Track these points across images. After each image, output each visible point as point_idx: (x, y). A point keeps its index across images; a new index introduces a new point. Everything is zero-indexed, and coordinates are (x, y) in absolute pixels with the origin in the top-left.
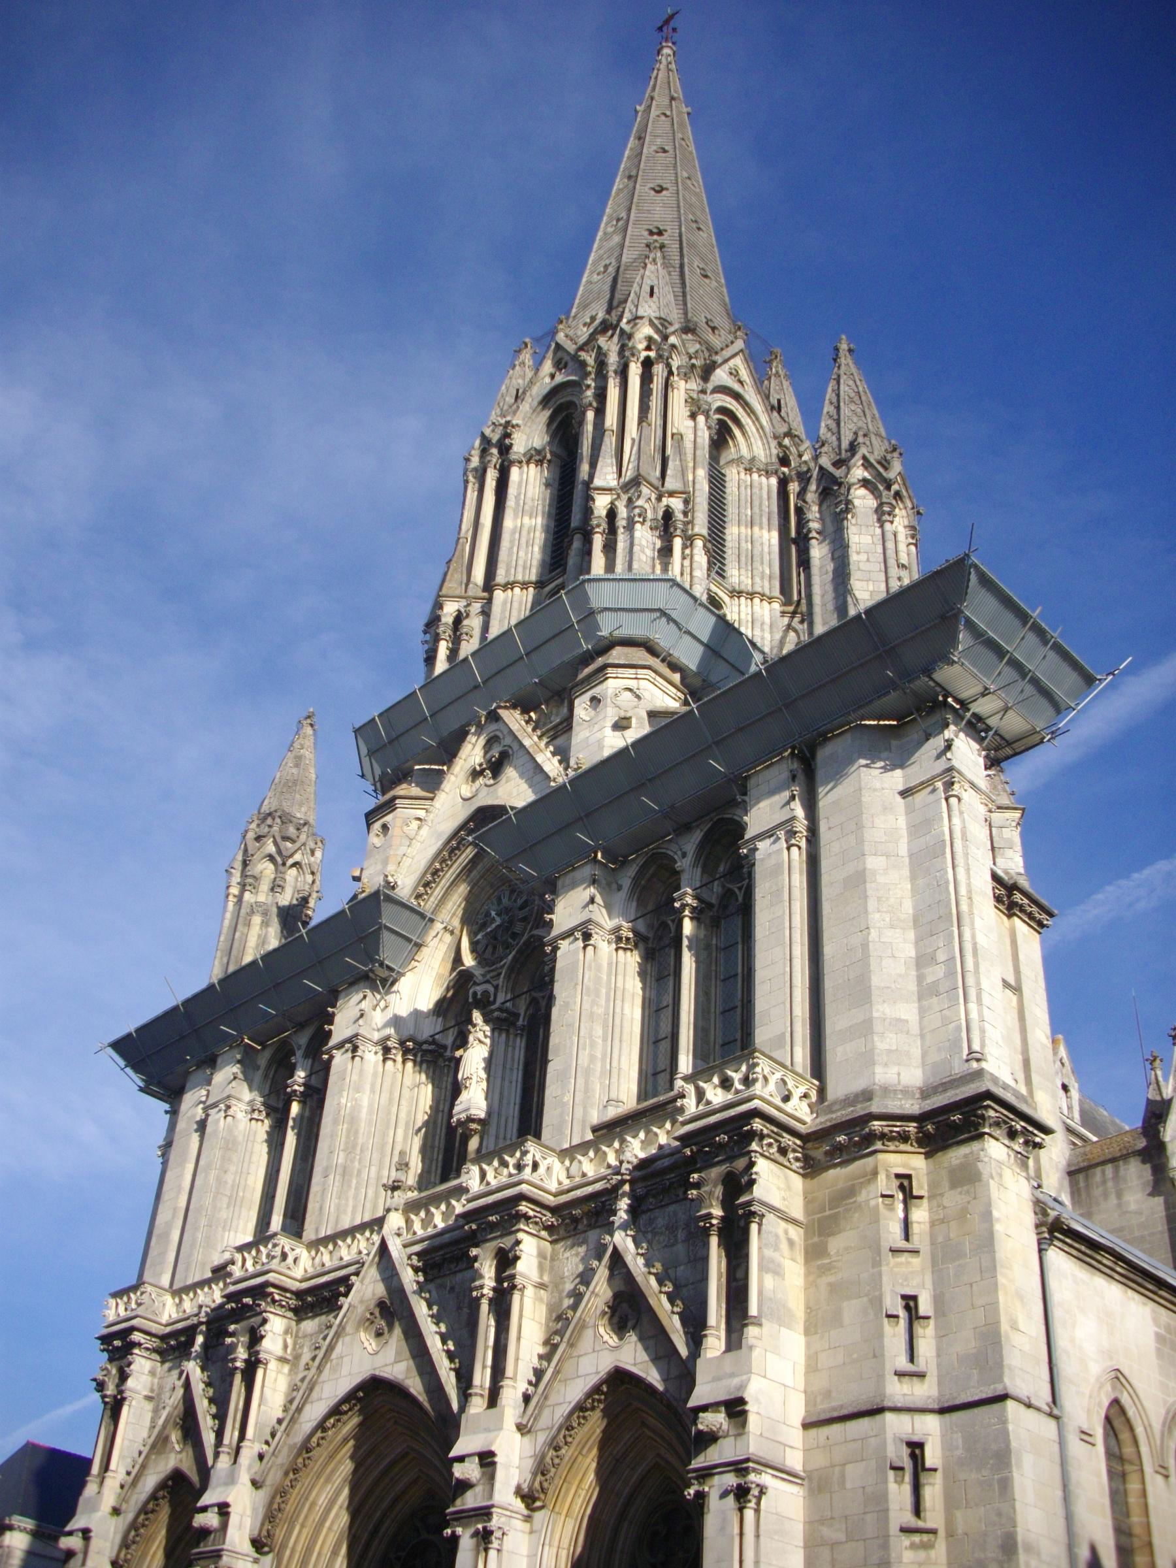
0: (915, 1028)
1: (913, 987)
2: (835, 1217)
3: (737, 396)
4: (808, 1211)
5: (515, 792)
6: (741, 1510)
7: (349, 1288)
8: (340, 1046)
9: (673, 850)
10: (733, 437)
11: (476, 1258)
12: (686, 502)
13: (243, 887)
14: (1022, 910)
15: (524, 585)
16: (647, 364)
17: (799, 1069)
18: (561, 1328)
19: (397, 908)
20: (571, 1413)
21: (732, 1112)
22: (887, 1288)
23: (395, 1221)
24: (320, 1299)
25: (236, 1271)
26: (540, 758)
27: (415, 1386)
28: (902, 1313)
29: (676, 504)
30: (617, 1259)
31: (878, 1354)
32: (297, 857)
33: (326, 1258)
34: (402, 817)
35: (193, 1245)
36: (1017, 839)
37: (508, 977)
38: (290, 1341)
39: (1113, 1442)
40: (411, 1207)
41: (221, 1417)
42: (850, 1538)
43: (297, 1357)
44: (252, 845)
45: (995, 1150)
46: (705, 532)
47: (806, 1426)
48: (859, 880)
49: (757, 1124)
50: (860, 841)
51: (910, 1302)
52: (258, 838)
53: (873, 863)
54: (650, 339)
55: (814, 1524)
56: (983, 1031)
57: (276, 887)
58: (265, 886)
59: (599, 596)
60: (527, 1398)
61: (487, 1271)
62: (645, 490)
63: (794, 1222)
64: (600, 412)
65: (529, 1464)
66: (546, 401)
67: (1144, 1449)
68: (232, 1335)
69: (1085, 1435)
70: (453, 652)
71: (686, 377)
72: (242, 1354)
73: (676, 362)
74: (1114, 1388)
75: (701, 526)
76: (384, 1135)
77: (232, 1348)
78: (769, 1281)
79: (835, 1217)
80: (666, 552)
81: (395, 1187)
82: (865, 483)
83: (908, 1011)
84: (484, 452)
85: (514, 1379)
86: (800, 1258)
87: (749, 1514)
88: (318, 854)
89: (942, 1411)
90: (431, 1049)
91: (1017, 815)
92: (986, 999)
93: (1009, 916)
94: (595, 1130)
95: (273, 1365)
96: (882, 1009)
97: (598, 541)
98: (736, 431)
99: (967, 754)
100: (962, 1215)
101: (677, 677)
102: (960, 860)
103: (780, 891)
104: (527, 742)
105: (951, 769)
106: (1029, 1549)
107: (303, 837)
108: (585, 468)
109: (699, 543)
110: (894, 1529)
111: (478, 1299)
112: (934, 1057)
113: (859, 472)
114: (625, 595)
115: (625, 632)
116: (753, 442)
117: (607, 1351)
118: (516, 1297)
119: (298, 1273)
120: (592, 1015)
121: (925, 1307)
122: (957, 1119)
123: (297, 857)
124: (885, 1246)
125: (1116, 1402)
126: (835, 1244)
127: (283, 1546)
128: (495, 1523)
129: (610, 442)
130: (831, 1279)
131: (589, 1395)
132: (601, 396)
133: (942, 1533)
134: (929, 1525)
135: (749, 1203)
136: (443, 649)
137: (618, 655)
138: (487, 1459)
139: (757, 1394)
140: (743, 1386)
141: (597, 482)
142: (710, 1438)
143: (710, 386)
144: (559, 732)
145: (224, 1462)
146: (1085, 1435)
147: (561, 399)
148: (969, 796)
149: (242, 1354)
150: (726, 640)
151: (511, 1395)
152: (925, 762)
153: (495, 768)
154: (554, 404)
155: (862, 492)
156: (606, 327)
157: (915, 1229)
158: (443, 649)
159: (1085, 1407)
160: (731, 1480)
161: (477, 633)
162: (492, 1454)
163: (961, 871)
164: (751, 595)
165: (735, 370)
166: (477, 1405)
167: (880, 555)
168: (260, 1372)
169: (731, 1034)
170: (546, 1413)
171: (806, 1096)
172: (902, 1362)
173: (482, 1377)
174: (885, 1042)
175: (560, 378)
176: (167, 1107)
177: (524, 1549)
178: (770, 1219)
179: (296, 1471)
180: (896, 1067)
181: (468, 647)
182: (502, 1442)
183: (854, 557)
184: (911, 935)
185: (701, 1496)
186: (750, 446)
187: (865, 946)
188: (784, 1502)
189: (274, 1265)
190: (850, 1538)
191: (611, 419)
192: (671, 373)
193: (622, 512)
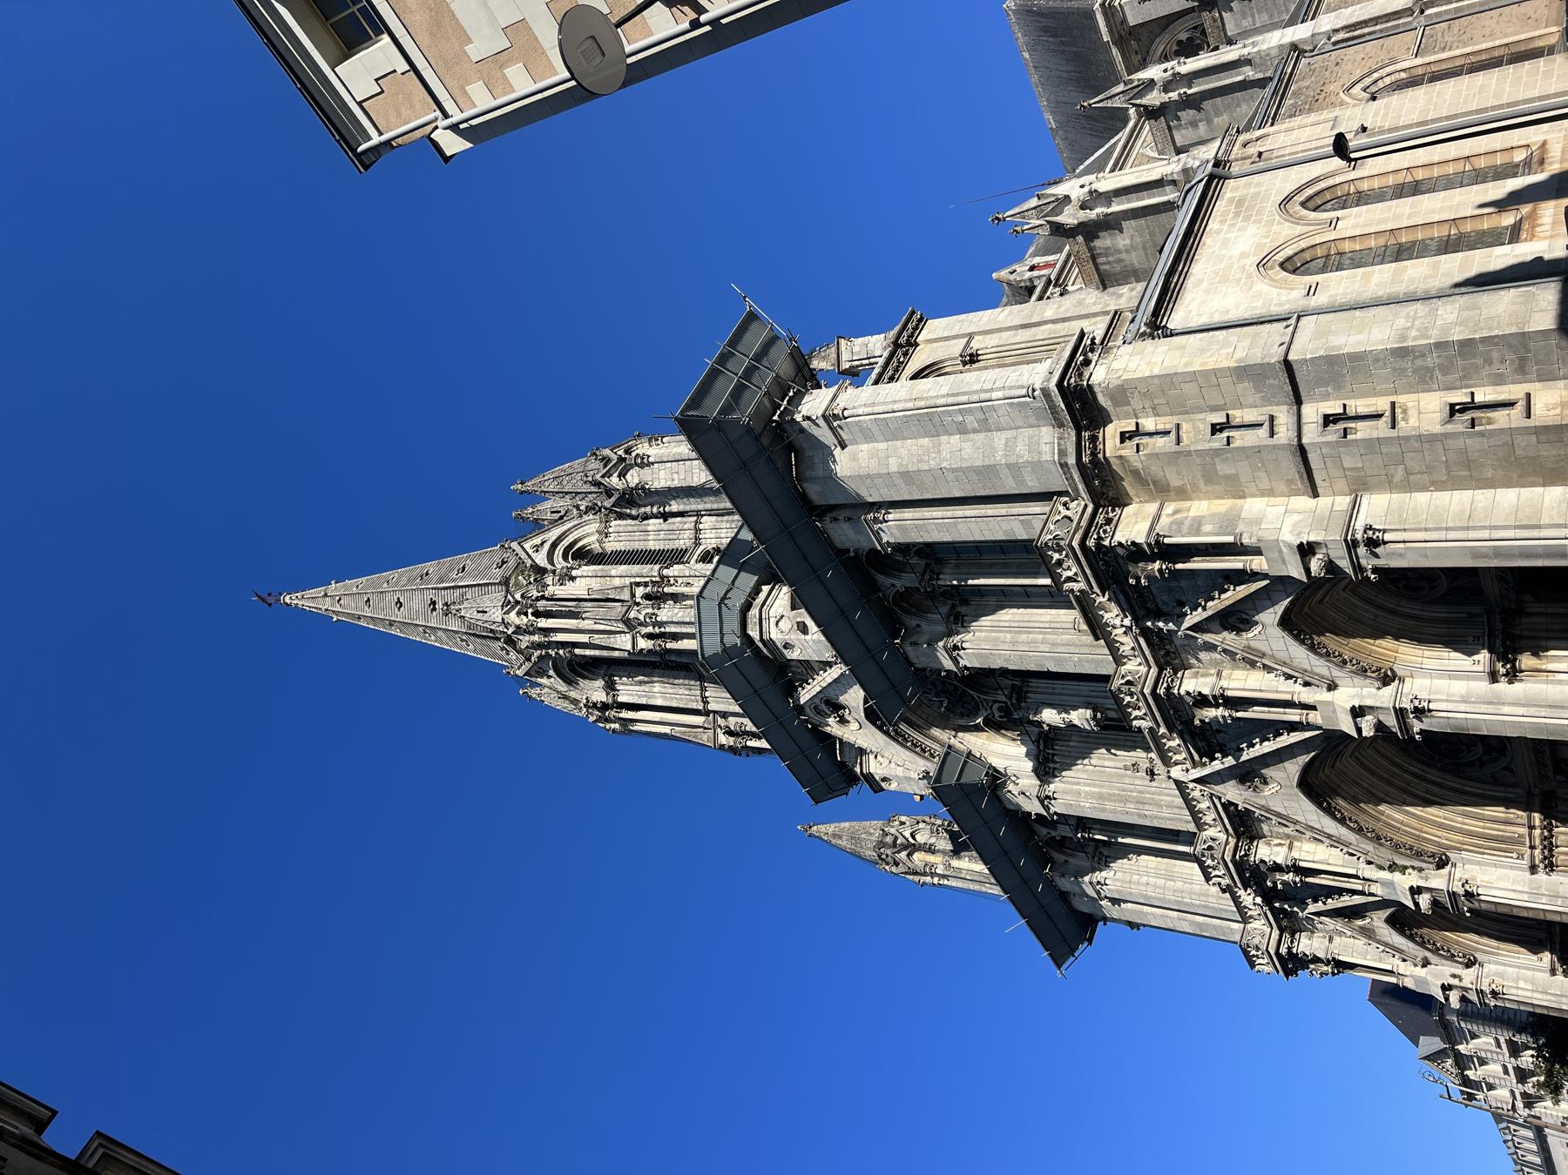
0: (1009, 434)
1: (981, 436)
2: (1154, 482)
3: (554, 545)
4: (1152, 500)
5: (854, 697)
6: (1385, 543)
7: (1230, 803)
8: (1047, 808)
9: (891, 593)
10: (584, 547)
11: (1202, 721)
12: (638, 584)
13: (933, 875)
14: (912, 335)
15: (703, 689)
16: (537, 614)
17: (1047, 509)
18: (1251, 661)
19: (944, 773)
20: (1317, 654)
21: (1082, 559)
22: (1207, 446)
23: (1176, 772)
24: (1244, 824)
25: (1226, 881)
26: (829, 680)
27: (1304, 759)
28: (1225, 434)
29: (640, 591)
30: (1196, 628)
31: (1258, 450)
32: (907, 834)
33: (1209, 818)
34: (875, 767)
35: (1206, 907)
36: (860, 340)
37: (986, 693)
38: (1277, 841)
39: (1329, 206)
40: (1167, 762)
41: (1340, 892)
42: (1403, 462)
43: (1288, 836)
44: (901, 869)
45: (1099, 375)
46: (657, 567)
47: (1315, 495)
48: (906, 475)
49: (1091, 543)
50: (880, 475)
51: (1216, 429)
52: (897, 864)
53: (894, 466)
54: (518, 614)
55: (1390, 486)
56: (1011, 388)
57: (930, 850)
58: (931, 858)
59: (713, 646)
60: (1307, 684)
61: (1210, 713)
62: (632, 615)
63: (1161, 508)
64: (575, 645)
65: (1358, 680)
66: (569, 682)
67: (1318, 239)
68: (1275, 883)
69: (1311, 291)
70: (754, 735)
71: (545, 586)
72: (1289, 877)
73: (536, 594)
74: (1272, 268)
75: (653, 570)
76: (1110, 774)
77: (1284, 883)
78: (1207, 528)
79: (1154, 482)
80: (676, 598)
81: (1151, 773)
82: (622, 475)
83: (999, 439)
84: (607, 720)
85: (1293, 694)
86: (1187, 504)
87: (1387, 537)
88: (903, 819)
89: (1298, 401)
90: (1051, 754)
91: (843, 342)
92: (988, 386)
93: (917, 345)
94: (1097, 639)
95: (1295, 854)
96: (1000, 457)
97: (671, 645)
98: (580, 544)
99: (814, 404)
100: (1146, 395)
101: (766, 588)
102: (889, 408)
103: (917, 526)
104: (818, 689)
105: (823, 416)
106: (1403, 337)
107: (893, 831)
108: (616, 654)
109: (665, 572)
110: (1394, 433)
111: (1234, 719)
112: (1033, 420)
113: (614, 480)
114: (711, 627)
115: (736, 627)
116: (588, 533)
117: (1267, 631)
118: (1229, 693)
119: (1223, 837)
120: (1013, 643)
121: (1219, 418)
122: (1080, 406)
123: (907, 834)
124: (1176, 448)
125: (1282, 265)
126: (1175, 482)
127: (1440, 845)
128: (1406, 705)
129: (598, 639)
130: (1202, 482)
131: (1302, 642)
132: (563, 645)
133: (1393, 398)
134: (1388, 407)
135: (1149, 545)
136: (753, 743)
137: (754, 633)
138: (1358, 712)
139: (1291, 536)
140: (1289, 546)
141: (629, 647)
142: (1330, 566)
143: (549, 567)
144: (809, 669)
145: (1375, 888)
146: (1311, 291)
147: (567, 671)
148: (842, 401)
149: (1289, 877)
150: (729, 555)
151: (1306, 695)
152: (824, 434)
153: (836, 707)
154: (571, 676)
155: (628, 476)
156: (510, 641)
157: (1161, 427)
158: (753, 743)
159: (1287, 293)
160: (1362, 550)
161: (740, 720)
162: (1353, 708)
163: (895, 407)
164: (697, 530)
165: (535, 550)
166: (1315, 717)
167: (671, 462)
168: (1302, 864)
169: (1024, 554)
170: (1317, 670)
171: (1065, 504)
172: (1263, 432)
173: (1293, 715)
174: (1022, 451)
175: (551, 672)
176: (1101, 924)
177: (1426, 682)
178: (1158, 529)
179: (1379, 838)
180: (1044, 446)
181: (750, 727)
182: (1343, 701)
183: (676, 483)
184: (944, 438)
185: (1375, 570)
186: (588, 535)
187: (954, 470)
188: (1376, 509)
189: (1218, 855)
190: (1403, 462)
191: (584, 638)
192: (543, 597)
193: (650, 629)
